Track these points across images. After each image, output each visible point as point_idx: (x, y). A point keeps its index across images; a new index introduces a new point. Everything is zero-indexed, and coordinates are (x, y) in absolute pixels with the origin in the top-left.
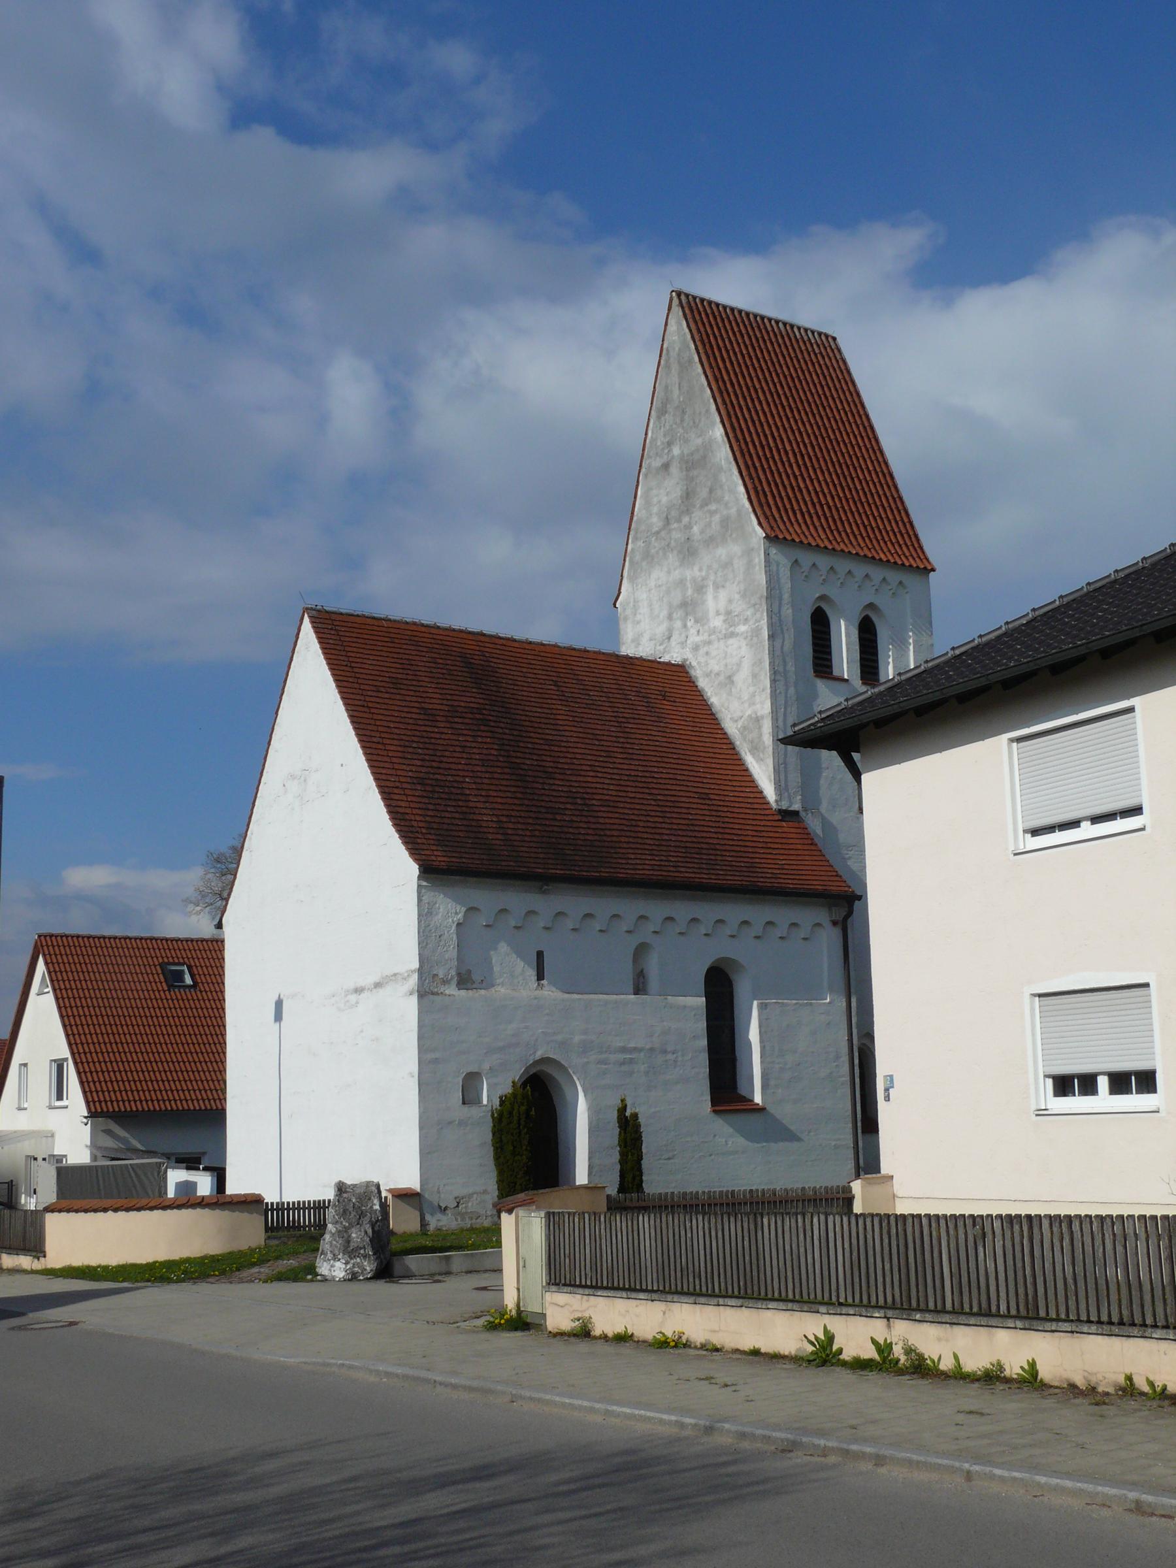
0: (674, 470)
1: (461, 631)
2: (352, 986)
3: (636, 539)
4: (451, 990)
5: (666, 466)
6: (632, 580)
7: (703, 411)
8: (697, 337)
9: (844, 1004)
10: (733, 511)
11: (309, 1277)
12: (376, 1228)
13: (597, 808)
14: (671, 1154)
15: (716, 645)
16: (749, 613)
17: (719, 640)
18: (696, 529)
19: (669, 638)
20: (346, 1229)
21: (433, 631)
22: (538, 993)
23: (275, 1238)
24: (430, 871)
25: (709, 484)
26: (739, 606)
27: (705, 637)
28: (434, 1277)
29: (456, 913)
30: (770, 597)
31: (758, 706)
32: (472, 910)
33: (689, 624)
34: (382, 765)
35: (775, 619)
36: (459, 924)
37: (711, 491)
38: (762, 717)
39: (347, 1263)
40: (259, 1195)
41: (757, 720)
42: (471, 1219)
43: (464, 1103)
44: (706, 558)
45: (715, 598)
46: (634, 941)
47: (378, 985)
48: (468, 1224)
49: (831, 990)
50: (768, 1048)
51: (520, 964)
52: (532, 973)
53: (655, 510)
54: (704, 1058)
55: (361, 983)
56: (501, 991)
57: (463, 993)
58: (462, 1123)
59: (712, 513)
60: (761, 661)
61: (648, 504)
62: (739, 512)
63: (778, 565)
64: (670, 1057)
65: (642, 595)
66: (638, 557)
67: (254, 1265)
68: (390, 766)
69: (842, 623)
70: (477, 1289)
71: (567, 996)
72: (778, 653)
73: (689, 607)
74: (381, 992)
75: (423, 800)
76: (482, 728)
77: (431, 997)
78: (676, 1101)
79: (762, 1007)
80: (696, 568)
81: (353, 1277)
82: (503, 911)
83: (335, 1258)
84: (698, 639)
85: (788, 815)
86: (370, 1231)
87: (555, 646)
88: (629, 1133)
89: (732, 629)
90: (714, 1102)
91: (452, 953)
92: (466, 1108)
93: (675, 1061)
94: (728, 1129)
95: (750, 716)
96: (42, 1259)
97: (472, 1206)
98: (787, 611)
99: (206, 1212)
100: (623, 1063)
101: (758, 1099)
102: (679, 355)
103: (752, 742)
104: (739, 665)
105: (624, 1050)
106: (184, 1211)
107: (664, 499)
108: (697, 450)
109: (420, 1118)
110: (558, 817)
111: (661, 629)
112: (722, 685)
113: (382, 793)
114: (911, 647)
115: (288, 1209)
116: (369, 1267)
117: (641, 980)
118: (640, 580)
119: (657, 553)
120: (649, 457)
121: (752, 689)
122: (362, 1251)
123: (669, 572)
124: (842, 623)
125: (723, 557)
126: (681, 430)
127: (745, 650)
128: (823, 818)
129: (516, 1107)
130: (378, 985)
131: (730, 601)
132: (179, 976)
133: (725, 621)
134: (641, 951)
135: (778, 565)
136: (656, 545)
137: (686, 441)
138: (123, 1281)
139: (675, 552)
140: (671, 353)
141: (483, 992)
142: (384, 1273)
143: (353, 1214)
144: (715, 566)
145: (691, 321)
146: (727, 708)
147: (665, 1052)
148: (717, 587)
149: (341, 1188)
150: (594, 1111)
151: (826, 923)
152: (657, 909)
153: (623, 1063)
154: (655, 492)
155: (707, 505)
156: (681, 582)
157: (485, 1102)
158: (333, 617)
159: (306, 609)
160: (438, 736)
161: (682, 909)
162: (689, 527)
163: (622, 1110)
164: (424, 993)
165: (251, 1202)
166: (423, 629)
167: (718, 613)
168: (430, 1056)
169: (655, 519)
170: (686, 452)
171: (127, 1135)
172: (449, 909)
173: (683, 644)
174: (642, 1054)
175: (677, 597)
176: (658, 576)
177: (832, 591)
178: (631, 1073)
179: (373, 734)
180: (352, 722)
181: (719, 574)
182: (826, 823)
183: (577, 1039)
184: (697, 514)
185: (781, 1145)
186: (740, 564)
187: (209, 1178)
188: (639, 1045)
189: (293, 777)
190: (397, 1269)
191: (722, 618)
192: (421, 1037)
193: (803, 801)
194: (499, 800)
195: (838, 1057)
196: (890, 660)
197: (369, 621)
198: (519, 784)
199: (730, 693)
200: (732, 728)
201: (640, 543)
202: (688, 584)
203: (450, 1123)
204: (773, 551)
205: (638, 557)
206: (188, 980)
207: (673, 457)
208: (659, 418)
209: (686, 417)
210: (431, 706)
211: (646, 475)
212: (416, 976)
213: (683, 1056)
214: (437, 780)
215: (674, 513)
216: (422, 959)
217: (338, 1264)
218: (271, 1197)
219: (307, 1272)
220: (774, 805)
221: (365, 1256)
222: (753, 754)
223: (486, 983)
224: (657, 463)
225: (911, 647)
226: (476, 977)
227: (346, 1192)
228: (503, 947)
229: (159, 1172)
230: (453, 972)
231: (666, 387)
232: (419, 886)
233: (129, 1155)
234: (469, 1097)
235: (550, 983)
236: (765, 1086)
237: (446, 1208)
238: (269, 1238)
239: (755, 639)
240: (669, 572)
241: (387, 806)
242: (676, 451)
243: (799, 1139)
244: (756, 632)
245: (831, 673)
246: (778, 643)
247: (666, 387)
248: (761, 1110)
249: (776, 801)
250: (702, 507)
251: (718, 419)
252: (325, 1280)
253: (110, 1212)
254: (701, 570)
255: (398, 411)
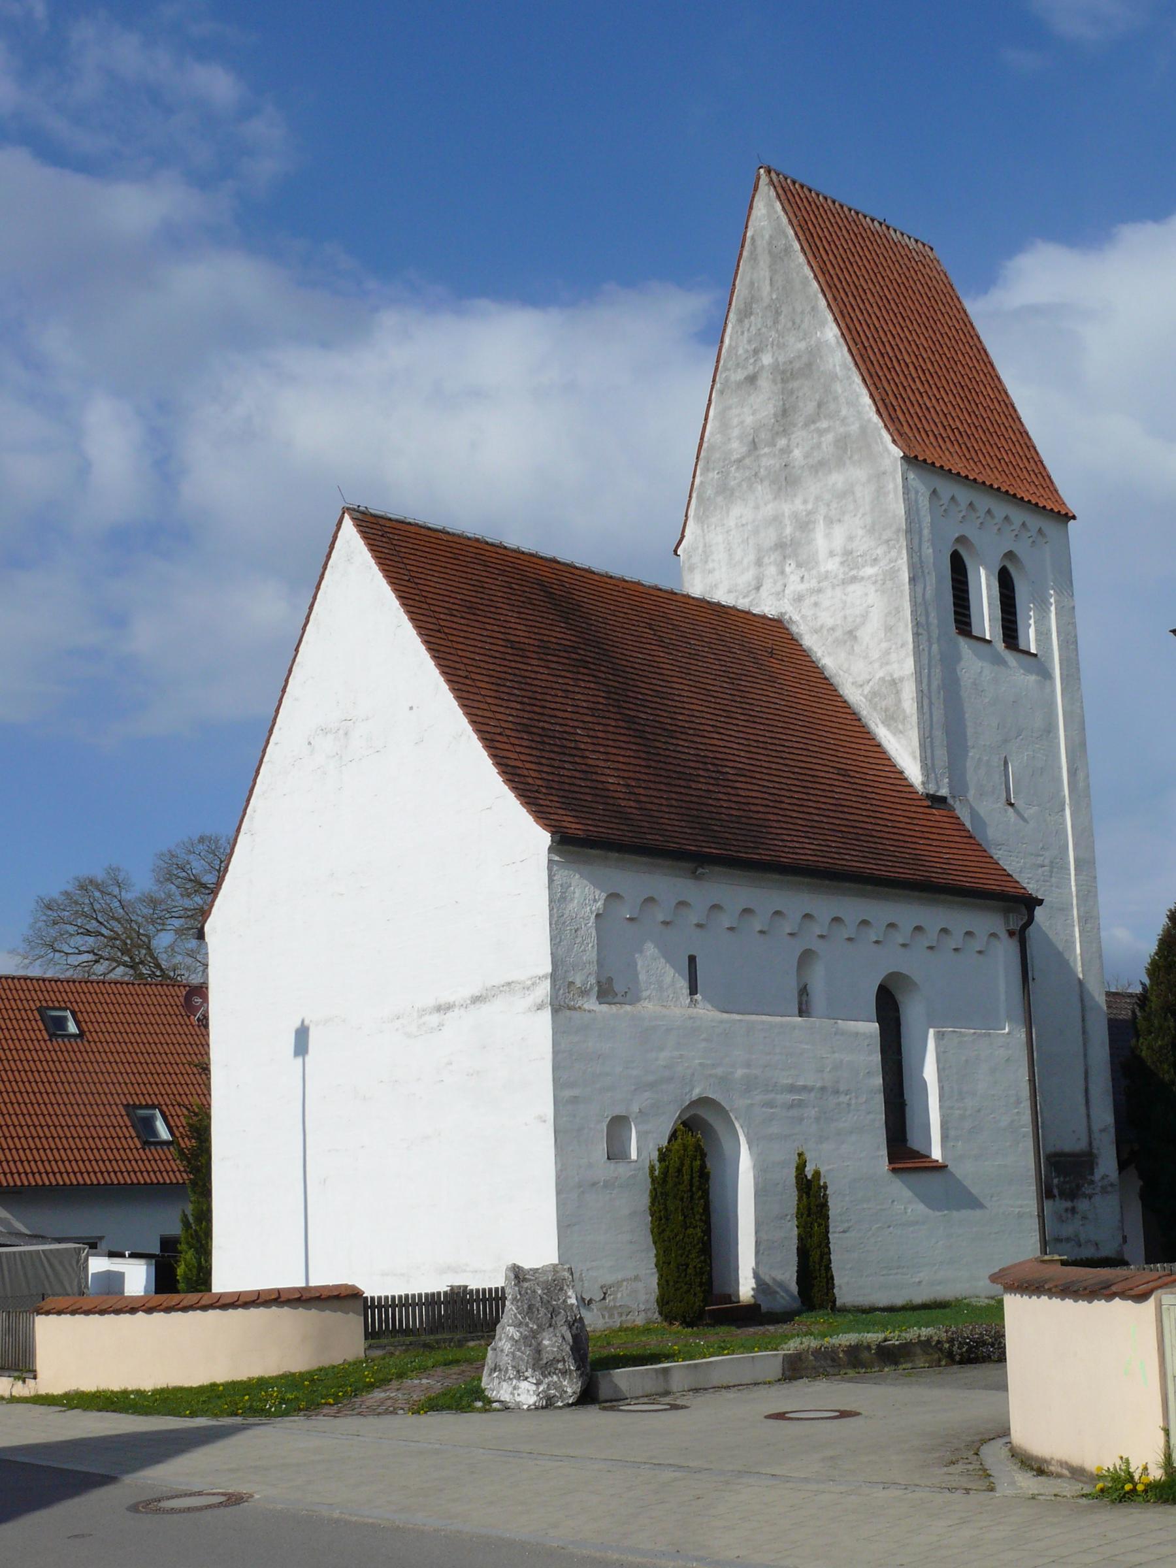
0: (764, 383)
1: (532, 555)
2: (431, 1002)
3: (707, 469)
4: (591, 1004)
5: (752, 379)
6: (700, 520)
7: (808, 309)
8: (795, 221)
9: (1024, 1035)
10: (854, 428)
11: (479, 1404)
12: (574, 1331)
13: (733, 778)
14: (846, 1225)
15: (829, 593)
16: (880, 551)
17: (833, 587)
18: (797, 453)
19: (758, 588)
20: (534, 1334)
21: (498, 550)
22: (693, 1011)
23: (379, 1347)
24: (567, 843)
25: (817, 397)
26: (863, 544)
27: (813, 583)
28: (662, 1397)
29: (595, 901)
30: (909, 531)
31: (895, 666)
32: (613, 897)
33: (788, 569)
34: (476, 704)
35: (916, 559)
36: (598, 916)
37: (819, 406)
38: (902, 679)
39: (538, 1384)
40: (353, 1287)
41: (894, 684)
42: (621, 1315)
43: (608, 1158)
44: (812, 487)
45: (828, 536)
46: (798, 947)
47: (477, 1000)
48: (617, 1322)
49: (1010, 1018)
50: (946, 1088)
51: (670, 971)
52: (683, 984)
53: (736, 432)
54: (880, 1099)
55: (446, 997)
56: (648, 1007)
57: (605, 1008)
58: (607, 1185)
59: (821, 432)
60: (898, 610)
61: (724, 426)
62: (863, 430)
63: (917, 492)
64: (844, 1099)
65: (717, 538)
66: (710, 492)
67: (371, 1387)
68: (486, 706)
69: (982, 572)
70: (769, 1417)
71: (725, 1016)
72: (919, 600)
73: (789, 549)
74: (484, 1009)
75: (534, 752)
76: (582, 670)
77: (568, 1012)
78: (853, 1156)
79: (940, 1036)
80: (798, 501)
81: (548, 1404)
82: (650, 900)
83: (520, 1376)
84: (802, 587)
85: (937, 801)
86: (569, 1336)
87: (639, 584)
88: (812, 1200)
89: (854, 572)
90: (891, 1160)
91: (591, 954)
92: (612, 1165)
93: (849, 1105)
94: (907, 1193)
95: (882, 679)
96: (30, 1382)
97: (621, 1297)
98: (928, 551)
99: (286, 1311)
100: (791, 1106)
101: (936, 1154)
102: (770, 243)
103: (886, 710)
104: (865, 616)
105: (792, 1089)
106: (253, 1311)
107: (749, 420)
108: (799, 357)
109: (558, 1177)
110: (694, 785)
111: (749, 575)
112: (838, 642)
113: (483, 739)
114: (1053, 608)
115: (394, 1306)
116: (571, 1387)
117: (804, 998)
118: (713, 520)
119: (740, 485)
120: (726, 369)
121: (884, 645)
122: (560, 1366)
123: (757, 507)
124: (982, 572)
125: (839, 485)
126: (773, 333)
127: (873, 597)
128: (971, 808)
129: (687, 1162)
130: (477, 1000)
131: (851, 538)
132: (60, 1023)
133: (842, 563)
134: (806, 958)
135: (917, 492)
136: (736, 475)
137: (782, 346)
138: (193, 1415)
139: (766, 483)
140: (759, 242)
141: (628, 1008)
142: (588, 1397)
143: (543, 1311)
144: (827, 497)
145: (786, 202)
146: (847, 671)
147: (837, 1092)
148: (830, 521)
149: (518, 1274)
150: (761, 1170)
151: (1003, 935)
152: (825, 906)
153: (791, 1106)
154: (734, 411)
155: (814, 422)
156: (776, 520)
157: (634, 1156)
158: (382, 522)
159: (346, 510)
160: (533, 675)
161: (853, 908)
162: (786, 451)
163: (801, 1167)
164: (560, 1006)
165: (329, 1298)
166: (489, 548)
167: (832, 554)
168: (568, 1093)
169: (735, 445)
170: (781, 359)
171: (8, 1216)
172: (587, 895)
173: (780, 595)
174: (813, 1095)
175: (769, 537)
176: (740, 513)
177: (971, 532)
178: (801, 1119)
179: (458, 666)
180: (429, 649)
181: (834, 505)
182: (974, 814)
183: (740, 1072)
184: (799, 434)
185: (966, 1213)
186: (864, 494)
187: (145, 1267)
188: (810, 1083)
189: (324, 731)
190: (604, 1391)
191: (838, 559)
192: (556, 1068)
193: (951, 787)
194: (621, 759)
195: (1018, 1102)
196: (1032, 621)
197: (423, 531)
198: (639, 741)
199: (851, 652)
200: (854, 695)
201: (713, 475)
202: (787, 522)
203: (594, 1184)
204: (911, 476)
205: (710, 492)
206: (72, 1028)
207: (763, 366)
208: (740, 321)
209: (782, 318)
210: (517, 639)
211: (722, 392)
212: (546, 985)
213: (857, 1098)
214: (543, 728)
215: (764, 435)
216: (556, 962)
217: (524, 1385)
218: (372, 1289)
219: (469, 1398)
220: (920, 789)
221: (564, 1373)
222: (888, 726)
223: (631, 996)
224: (739, 375)
225: (1053, 608)
226: (619, 987)
227: (525, 1280)
228: (650, 949)
229: (78, 1261)
230: (592, 980)
231: (752, 283)
232: (550, 861)
233: (14, 1240)
234: (616, 1153)
235: (704, 998)
236: (945, 1138)
237: (590, 1301)
238: (370, 1347)
239: (889, 584)
240: (757, 507)
241: (493, 756)
242: (767, 359)
243: (981, 1206)
244: (892, 574)
245: (971, 631)
246: (919, 589)
247: (752, 283)
248: (940, 1168)
249: (923, 783)
250: (806, 425)
251: (830, 317)
252: (506, 1408)
253: (140, 1314)
254: (805, 502)
255: (163, 462)
